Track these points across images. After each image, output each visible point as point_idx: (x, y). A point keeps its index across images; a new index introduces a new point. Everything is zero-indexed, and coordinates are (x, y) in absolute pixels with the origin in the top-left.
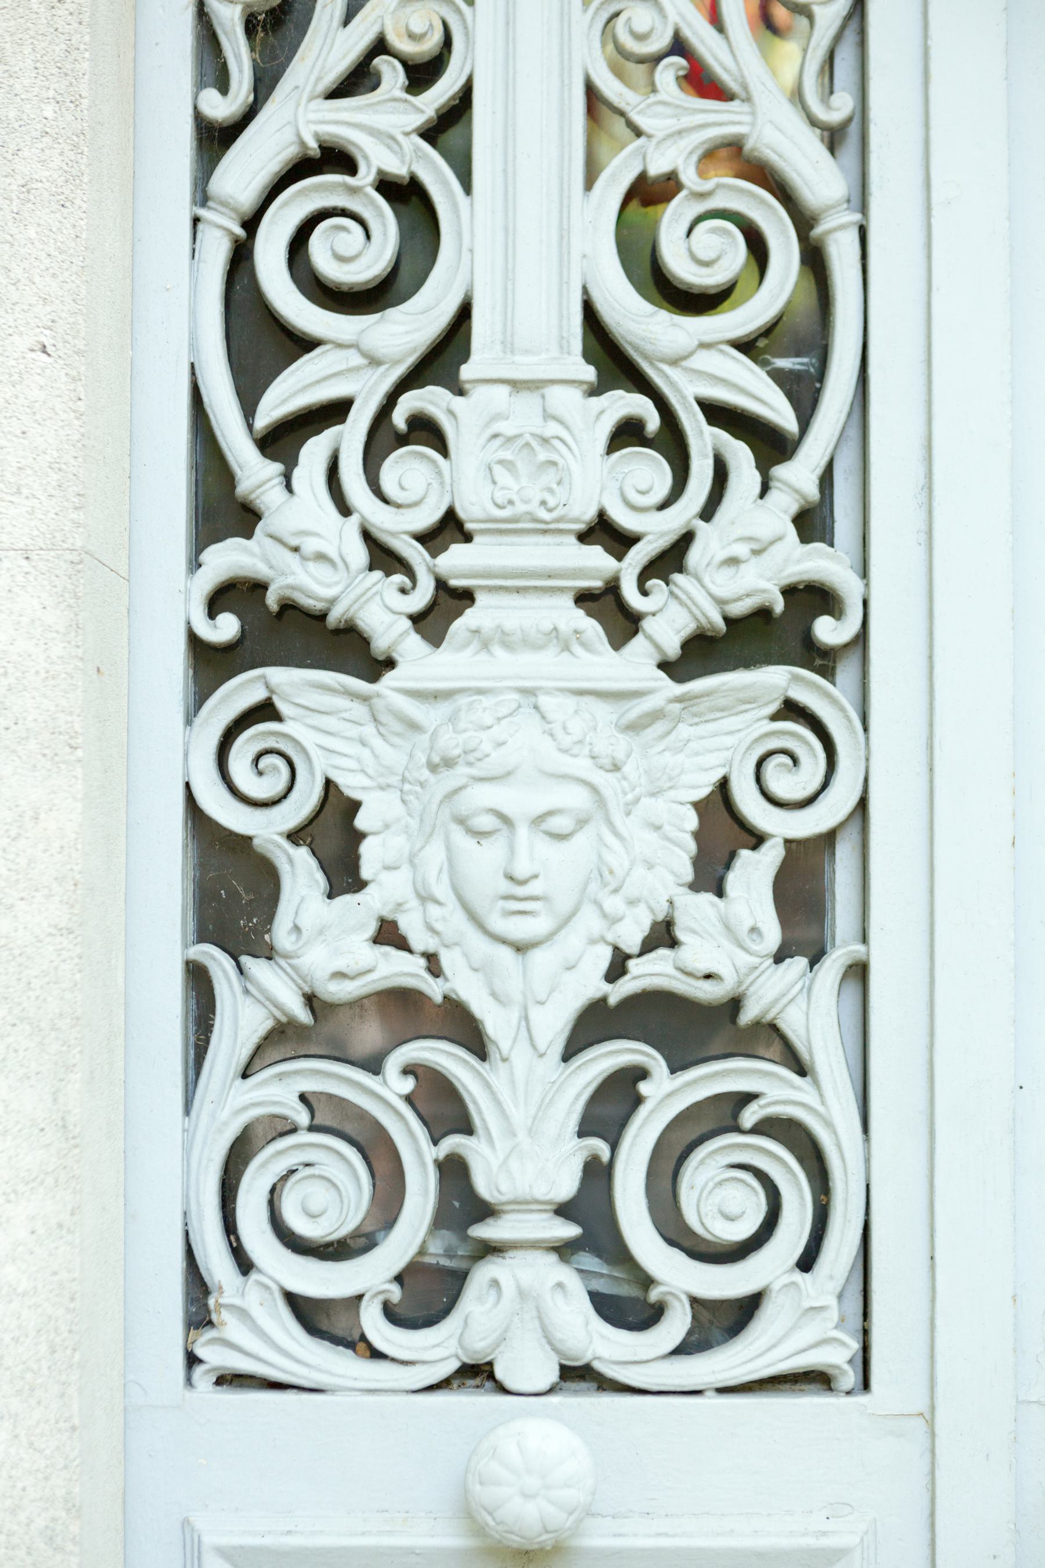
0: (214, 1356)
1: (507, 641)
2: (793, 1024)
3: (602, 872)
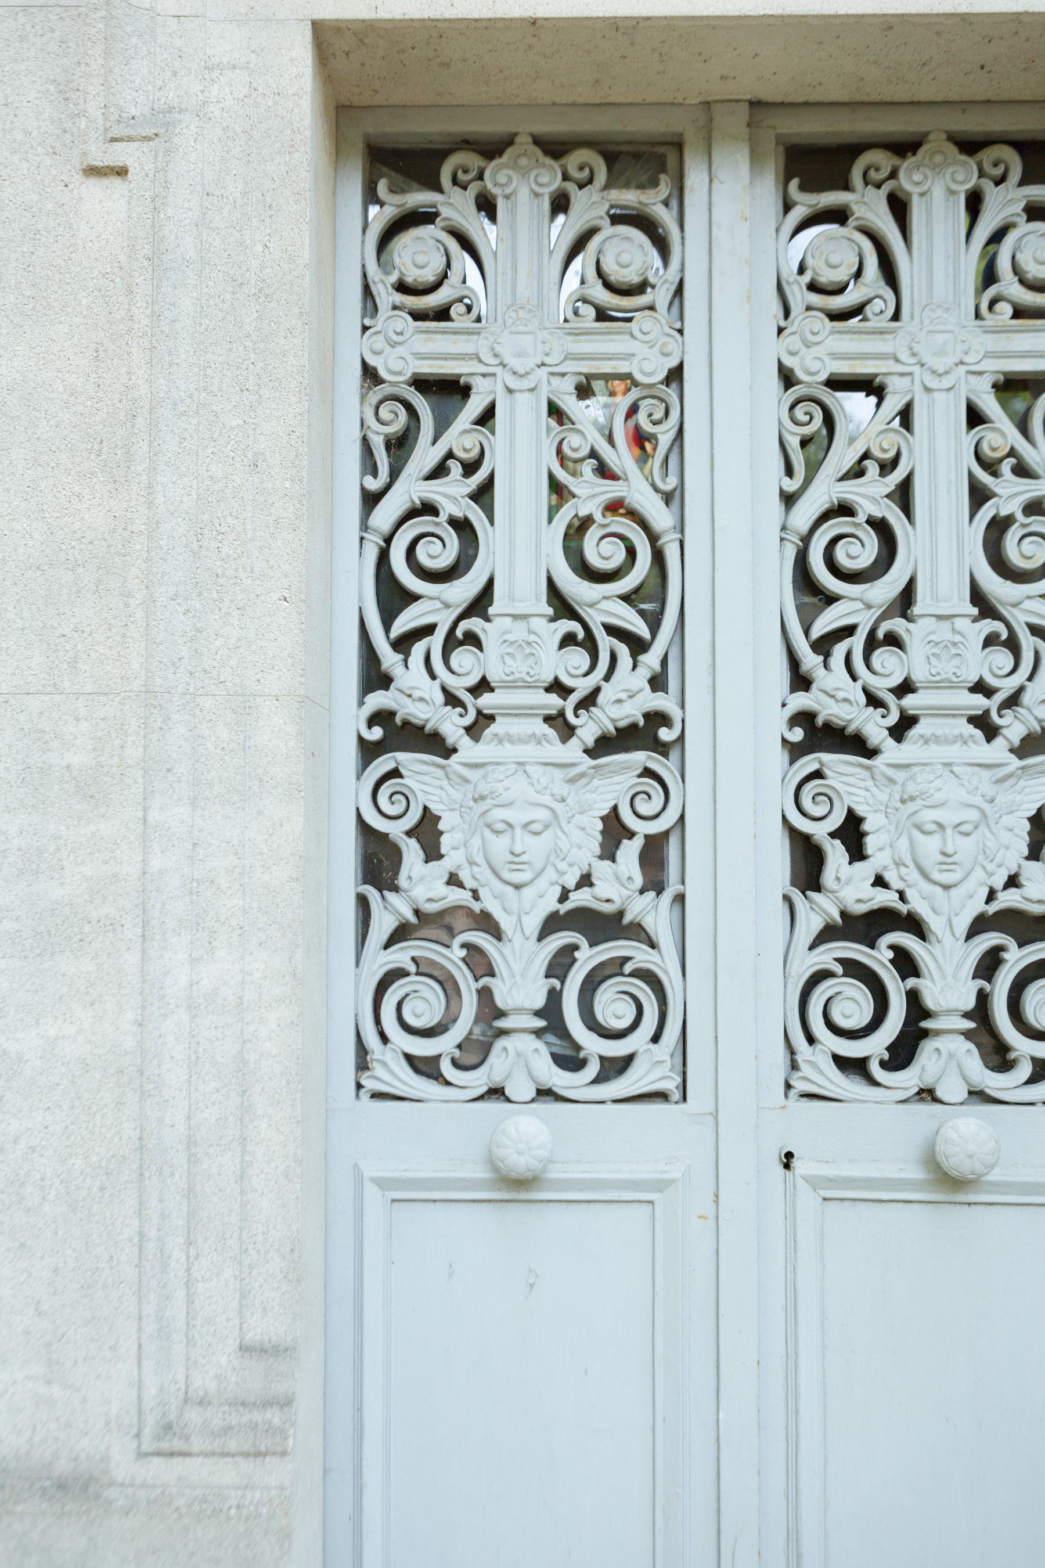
0: (369, 1084)
1: (511, 739)
2: (648, 923)
3: (556, 850)
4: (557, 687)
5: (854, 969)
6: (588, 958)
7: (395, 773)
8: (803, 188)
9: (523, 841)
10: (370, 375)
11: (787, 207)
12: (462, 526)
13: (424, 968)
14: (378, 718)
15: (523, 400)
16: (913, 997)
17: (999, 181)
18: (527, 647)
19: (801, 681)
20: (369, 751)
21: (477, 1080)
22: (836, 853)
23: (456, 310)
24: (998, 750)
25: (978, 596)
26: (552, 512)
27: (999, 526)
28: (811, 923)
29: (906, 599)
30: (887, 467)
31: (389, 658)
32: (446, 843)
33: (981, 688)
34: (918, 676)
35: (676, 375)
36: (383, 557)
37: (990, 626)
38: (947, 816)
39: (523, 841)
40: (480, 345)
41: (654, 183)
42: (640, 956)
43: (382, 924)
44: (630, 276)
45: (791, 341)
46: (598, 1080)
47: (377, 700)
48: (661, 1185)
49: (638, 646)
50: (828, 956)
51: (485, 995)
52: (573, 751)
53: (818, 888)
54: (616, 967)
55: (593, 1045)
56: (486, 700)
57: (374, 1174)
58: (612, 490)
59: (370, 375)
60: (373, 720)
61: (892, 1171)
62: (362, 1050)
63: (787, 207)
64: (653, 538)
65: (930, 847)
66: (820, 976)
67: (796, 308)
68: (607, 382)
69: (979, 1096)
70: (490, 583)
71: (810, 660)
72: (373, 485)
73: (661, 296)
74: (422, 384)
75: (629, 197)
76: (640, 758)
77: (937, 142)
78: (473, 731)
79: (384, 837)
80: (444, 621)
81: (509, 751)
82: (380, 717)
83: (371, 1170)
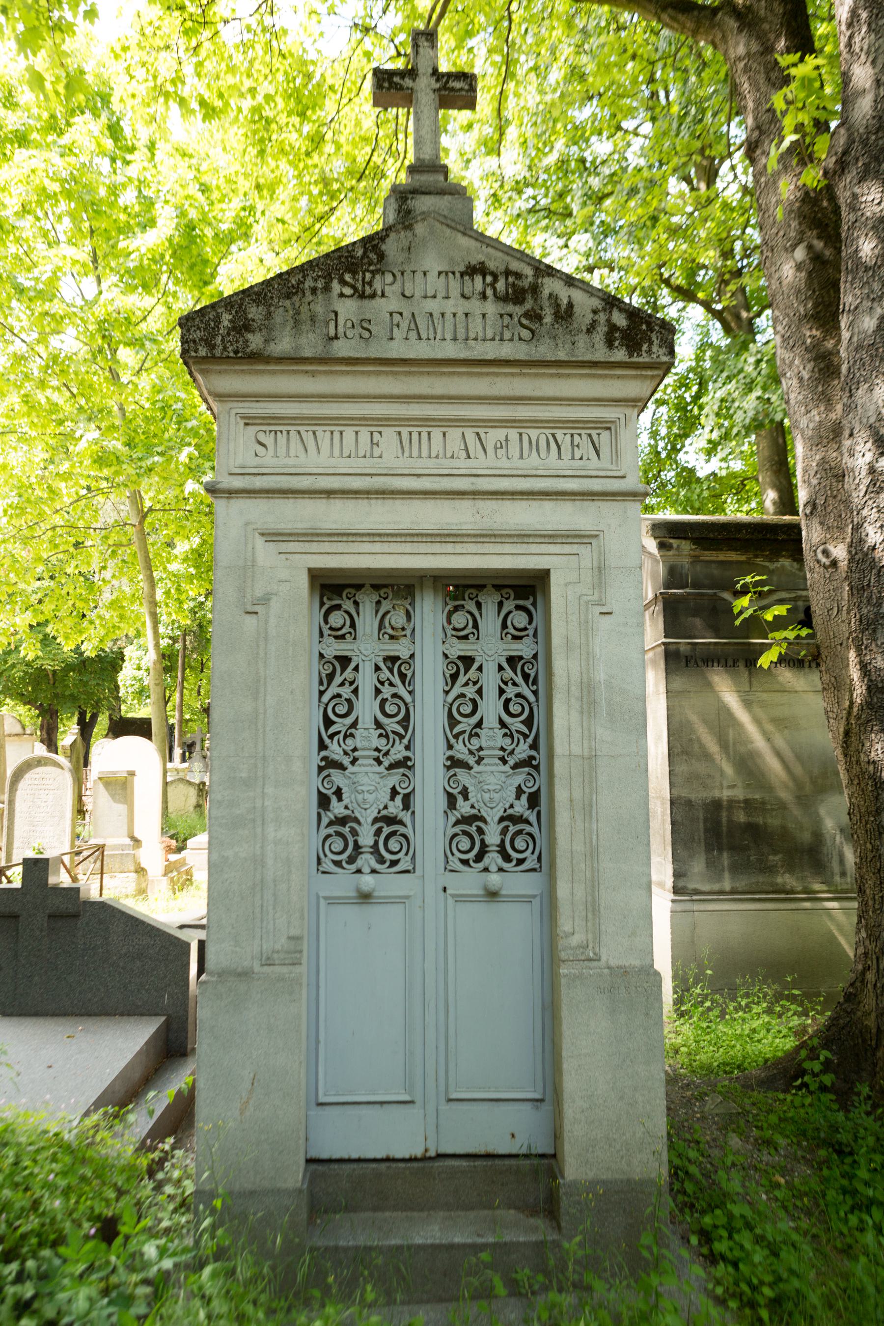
0: (321, 869)
1: (363, 765)
2: (404, 820)
3: (377, 798)
4: (502, 749)
5: (465, 833)
6: (386, 830)
7: (329, 776)
8: (329, 599)
9: (367, 796)
10: (321, 656)
11: (446, 604)
12: (349, 701)
13: (465, 833)
14: (324, 759)
15: (367, 664)
16: (483, 841)
17: (385, 599)
19: (450, 747)
20: (321, 769)
21: (353, 867)
22: (460, 799)
23: (348, 636)
24: (507, 768)
26: (500, 696)
28: (453, 820)
30: (475, 683)
31: (327, 741)
32: (344, 796)
33: (377, 750)
34: (484, 746)
35: (535, 656)
36: (325, 710)
37: (505, 731)
38: (491, 787)
39: (367, 796)
40: (355, 647)
41: (528, 599)
42: (528, 828)
43: (325, 821)
44: (521, 626)
45: (447, 645)
46: (389, 867)
47: (324, 753)
48: (407, 897)
49: (401, 737)
50: (457, 829)
51: (356, 842)
52: (381, 769)
53: (455, 809)
55: (514, 855)
56: (356, 754)
57: (327, 894)
58: (393, 690)
59: (321, 656)
60: (322, 760)
61: (475, 892)
62: (319, 859)
63: (322, 604)
64: (530, 704)
65: (360, 797)
66: (455, 835)
67: (449, 635)
69: (501, 870)
70: (482, 719)
71: (453, 741)
72: (322, 688)
73: (408, 632)
75: (521, 602)
76: (401, 770)
77: (489, 587)
78: (478, 762)
79: (325, 795)
80: (468, 729)
81: (363, 769)
82: (450, 758)
83: (321, 894)
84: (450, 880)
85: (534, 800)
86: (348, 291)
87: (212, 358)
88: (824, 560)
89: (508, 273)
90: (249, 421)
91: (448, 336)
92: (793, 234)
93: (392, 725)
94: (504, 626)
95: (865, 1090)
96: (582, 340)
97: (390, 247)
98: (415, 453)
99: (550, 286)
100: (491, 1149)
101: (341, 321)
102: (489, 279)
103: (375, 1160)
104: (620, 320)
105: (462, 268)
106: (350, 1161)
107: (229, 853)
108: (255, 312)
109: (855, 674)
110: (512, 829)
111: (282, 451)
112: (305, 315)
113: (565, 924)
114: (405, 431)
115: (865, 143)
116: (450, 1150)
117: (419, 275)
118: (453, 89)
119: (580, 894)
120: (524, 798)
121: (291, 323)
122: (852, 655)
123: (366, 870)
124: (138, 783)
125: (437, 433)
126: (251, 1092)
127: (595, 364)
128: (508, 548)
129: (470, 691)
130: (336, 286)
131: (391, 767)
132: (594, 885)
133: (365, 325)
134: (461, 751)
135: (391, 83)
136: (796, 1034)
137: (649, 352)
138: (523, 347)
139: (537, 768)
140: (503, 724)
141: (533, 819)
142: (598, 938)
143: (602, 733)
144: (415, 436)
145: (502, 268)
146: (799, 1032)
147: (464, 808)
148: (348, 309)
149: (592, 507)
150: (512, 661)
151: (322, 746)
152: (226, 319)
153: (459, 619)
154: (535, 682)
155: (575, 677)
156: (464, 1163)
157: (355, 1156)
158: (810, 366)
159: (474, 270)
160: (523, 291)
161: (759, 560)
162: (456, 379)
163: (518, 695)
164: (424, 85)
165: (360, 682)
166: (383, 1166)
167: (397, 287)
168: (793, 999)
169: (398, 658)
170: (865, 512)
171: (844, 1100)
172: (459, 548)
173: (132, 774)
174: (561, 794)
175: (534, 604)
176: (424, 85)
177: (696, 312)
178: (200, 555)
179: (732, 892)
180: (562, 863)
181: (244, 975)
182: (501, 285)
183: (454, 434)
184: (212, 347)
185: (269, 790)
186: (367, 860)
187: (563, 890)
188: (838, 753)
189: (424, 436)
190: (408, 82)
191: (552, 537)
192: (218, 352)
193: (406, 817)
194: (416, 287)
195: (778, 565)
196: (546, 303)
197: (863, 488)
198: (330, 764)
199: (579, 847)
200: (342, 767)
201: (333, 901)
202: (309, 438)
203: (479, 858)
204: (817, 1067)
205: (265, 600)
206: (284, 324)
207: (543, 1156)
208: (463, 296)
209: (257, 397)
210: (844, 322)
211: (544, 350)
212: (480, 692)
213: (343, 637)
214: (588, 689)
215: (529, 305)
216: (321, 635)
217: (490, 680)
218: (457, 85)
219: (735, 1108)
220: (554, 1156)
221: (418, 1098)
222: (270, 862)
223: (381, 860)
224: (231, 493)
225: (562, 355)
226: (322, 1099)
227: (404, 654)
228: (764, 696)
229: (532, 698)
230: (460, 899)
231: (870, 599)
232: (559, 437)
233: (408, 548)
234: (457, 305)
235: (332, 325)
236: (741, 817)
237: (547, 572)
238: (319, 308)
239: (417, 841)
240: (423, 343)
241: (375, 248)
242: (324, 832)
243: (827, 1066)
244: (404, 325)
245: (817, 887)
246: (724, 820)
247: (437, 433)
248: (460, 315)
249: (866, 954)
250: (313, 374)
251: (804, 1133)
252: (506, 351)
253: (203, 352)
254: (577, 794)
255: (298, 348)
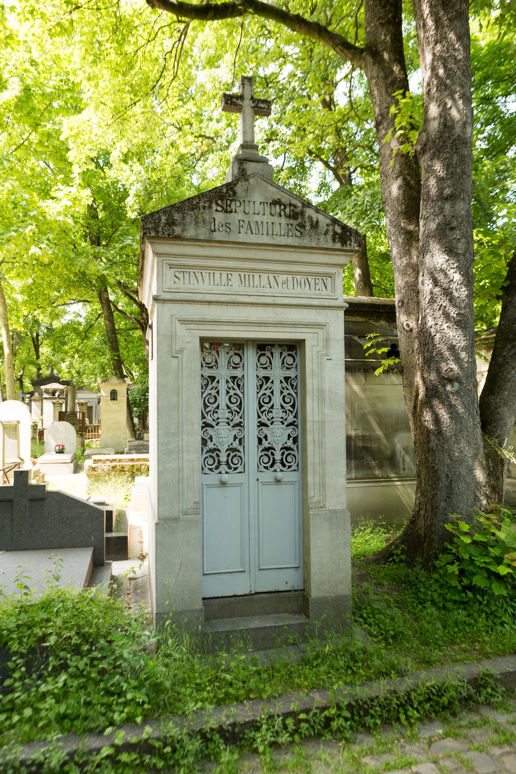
5: (266, 455)
10: (202, 376)
13: (211, 456)
18: (224, 413)
19: (259, 417)
21: (218, 471)
22: (264, 440)
25: (228, 406)
27: (284, 397)
28: (261, 449)
29: (218, 406)
31: (205, 415)
33: (228, 419)
35: (296, 377)
42: (293, 452)
43: (205, 451)
49: (238, 413)
50: (263, 453)
52: (230, 427)
54: (235, 455)
55: (287, 464)
58: (235, 392)
59: (202, 376)
65: (221, 440)
68: (39, 375)
69: (281, 471)
73: (241, 365)
74: (209, 377)
78: (217, 425)
82: (259, 422)
84: (260, 475)
85: (295, 440)
86: (220, 209)
87: (157, 237)
88: (407, 328)
89: (291, 205)
90: (171, 266)
91: (265, 233)
92: (396, 171)
93: (234, 407)
94: (283, 363)
95: (420, 560)
96: (322, 238)
97: (239, 189)
98: (247, 285)
99: (309, 212)
100: (278, 589)
101: (217, 223)
102: (282, 207)
103: (229, 597)
104: (338, 230)
105: (271, 201)
106: (218, 598)
107: (167, 466)
108: (177, 216)
109: (420, 382)
110: (286, 453)
111: (187, 281)
112: (200, 219)
113: (311, 493)
114: (242, 274)
115: (434, 142)
116: (260, 591)
117: (251, 203)
118: (260, 108)
119: (317, 480)
120: (291, 439)
121: (194, 223)
122: (419, 374)
123: (224, 472)
124: (21, 426)
125: (256, 276)
126: (180, 569)
127: (327, 249)
128: (287, 330)
129: (268, 392)
130: (214, 205)
131: (234, 426)
132: (323, 476)
133: (227, 225)
134: (264, 419)
135: (231, 101)
136: (386, 541)
137: (350, 245)
138: (297, 240)
139: (297, 426)
140: (282, 407)
141: (295, 448)
142: (325, 498)
143: (327, 411)
144: (247, 277)
145: (288, 202)
146: (387, 540)
147: (265, 444)
148: (220, 217)
149: (324, 312)
150: (287, 379)
151: (203, 417)
152: (164, 218)
153: (263, 360)
154: (296, 388)
155: (316, 387)
156: (267, 595)
157: (220, 595)
158: (403, 236)
159: (276, 202)
160: (297, 214)
161: (371, 321)
162: (267, 252)
163: (289, 394)
164: (247, 104)
165: (220, 388)
166: (233, 599)
167: (242, 208)
168: (382, 526)
169: (236, 377)
170: (428, 311)
171: (410, 564)
172: (266, 329)
173: (18, 422)
174: (309, 438)
175: (296, 354)
176: (247, 104)
177: (319, 165)
178: (32, 289)
179: (356, 479)
180: (310, 467)
181: (175, 519)
182: (287, 210)
183: (264, 276)
184: (158, 232)
185: (185, 438)
186: (224, 468)
187: (310, 479)
188: (410, 416)
189: (251, 277)
190: (239, 102)
191: (307, 325)
192: (160, 234)
193: (241, 448)
194: (250, 209)
195: (379, 324)
196: (307, 220)
197: (427, 300)
198: (206, 425)
199: (317, 460)
200: (212, 427)
201: (209, 486)
202: (199, 276)
203: (272, 466)
204: (399, 552)
205: (181, 351)
206: (191, 223)
207: (301, 590)
208: (271, 214)
209: (176, 255)
210: (421, 223)
211: (306, 242)
212: (272, 392)
213: (212, 367)
214: (321, 393)
215: (300, 220)
216: (202, 366)
217: (277, 387)
218: (263, 105)
219: (364, 572)
220: (304, 590)
221: (247, 570)
222: (185, 469)
223: (230, 468)
224: (165, 301)
225: (314, 244)
226: (206, 572)
227: (240, 375)
228: (372, 386)
229: (295, 395)
230: (264, 484)
231: (428, 349)
232: (310, 280)
233: (244, 328)
234: (267, 218)
235: (213, 224)
236: (360, 444)
237: (304, 341)
238: (207, 216)
239: (246, 459)
240: (254, 235)
241: (232, 189)
242: (205, 456)
243: (403, 550)
244: (245, 226)
245: (392, 475)
246: (353, 445)
247: (256, 276)
248: (270, 223)
249: (420, 503)
250: (203, 247)
251: (394, 580)
252: (290, 241)
253: (153, 234)
254: (316, 438)
255: (197, 235)
